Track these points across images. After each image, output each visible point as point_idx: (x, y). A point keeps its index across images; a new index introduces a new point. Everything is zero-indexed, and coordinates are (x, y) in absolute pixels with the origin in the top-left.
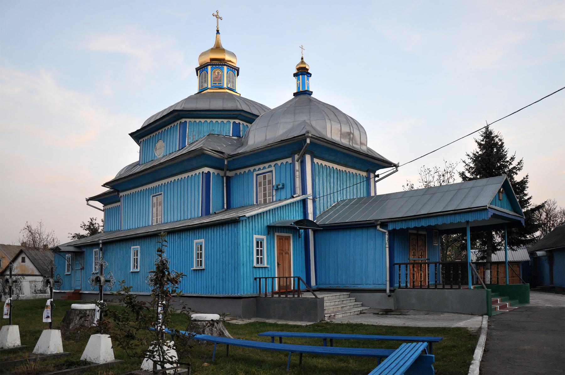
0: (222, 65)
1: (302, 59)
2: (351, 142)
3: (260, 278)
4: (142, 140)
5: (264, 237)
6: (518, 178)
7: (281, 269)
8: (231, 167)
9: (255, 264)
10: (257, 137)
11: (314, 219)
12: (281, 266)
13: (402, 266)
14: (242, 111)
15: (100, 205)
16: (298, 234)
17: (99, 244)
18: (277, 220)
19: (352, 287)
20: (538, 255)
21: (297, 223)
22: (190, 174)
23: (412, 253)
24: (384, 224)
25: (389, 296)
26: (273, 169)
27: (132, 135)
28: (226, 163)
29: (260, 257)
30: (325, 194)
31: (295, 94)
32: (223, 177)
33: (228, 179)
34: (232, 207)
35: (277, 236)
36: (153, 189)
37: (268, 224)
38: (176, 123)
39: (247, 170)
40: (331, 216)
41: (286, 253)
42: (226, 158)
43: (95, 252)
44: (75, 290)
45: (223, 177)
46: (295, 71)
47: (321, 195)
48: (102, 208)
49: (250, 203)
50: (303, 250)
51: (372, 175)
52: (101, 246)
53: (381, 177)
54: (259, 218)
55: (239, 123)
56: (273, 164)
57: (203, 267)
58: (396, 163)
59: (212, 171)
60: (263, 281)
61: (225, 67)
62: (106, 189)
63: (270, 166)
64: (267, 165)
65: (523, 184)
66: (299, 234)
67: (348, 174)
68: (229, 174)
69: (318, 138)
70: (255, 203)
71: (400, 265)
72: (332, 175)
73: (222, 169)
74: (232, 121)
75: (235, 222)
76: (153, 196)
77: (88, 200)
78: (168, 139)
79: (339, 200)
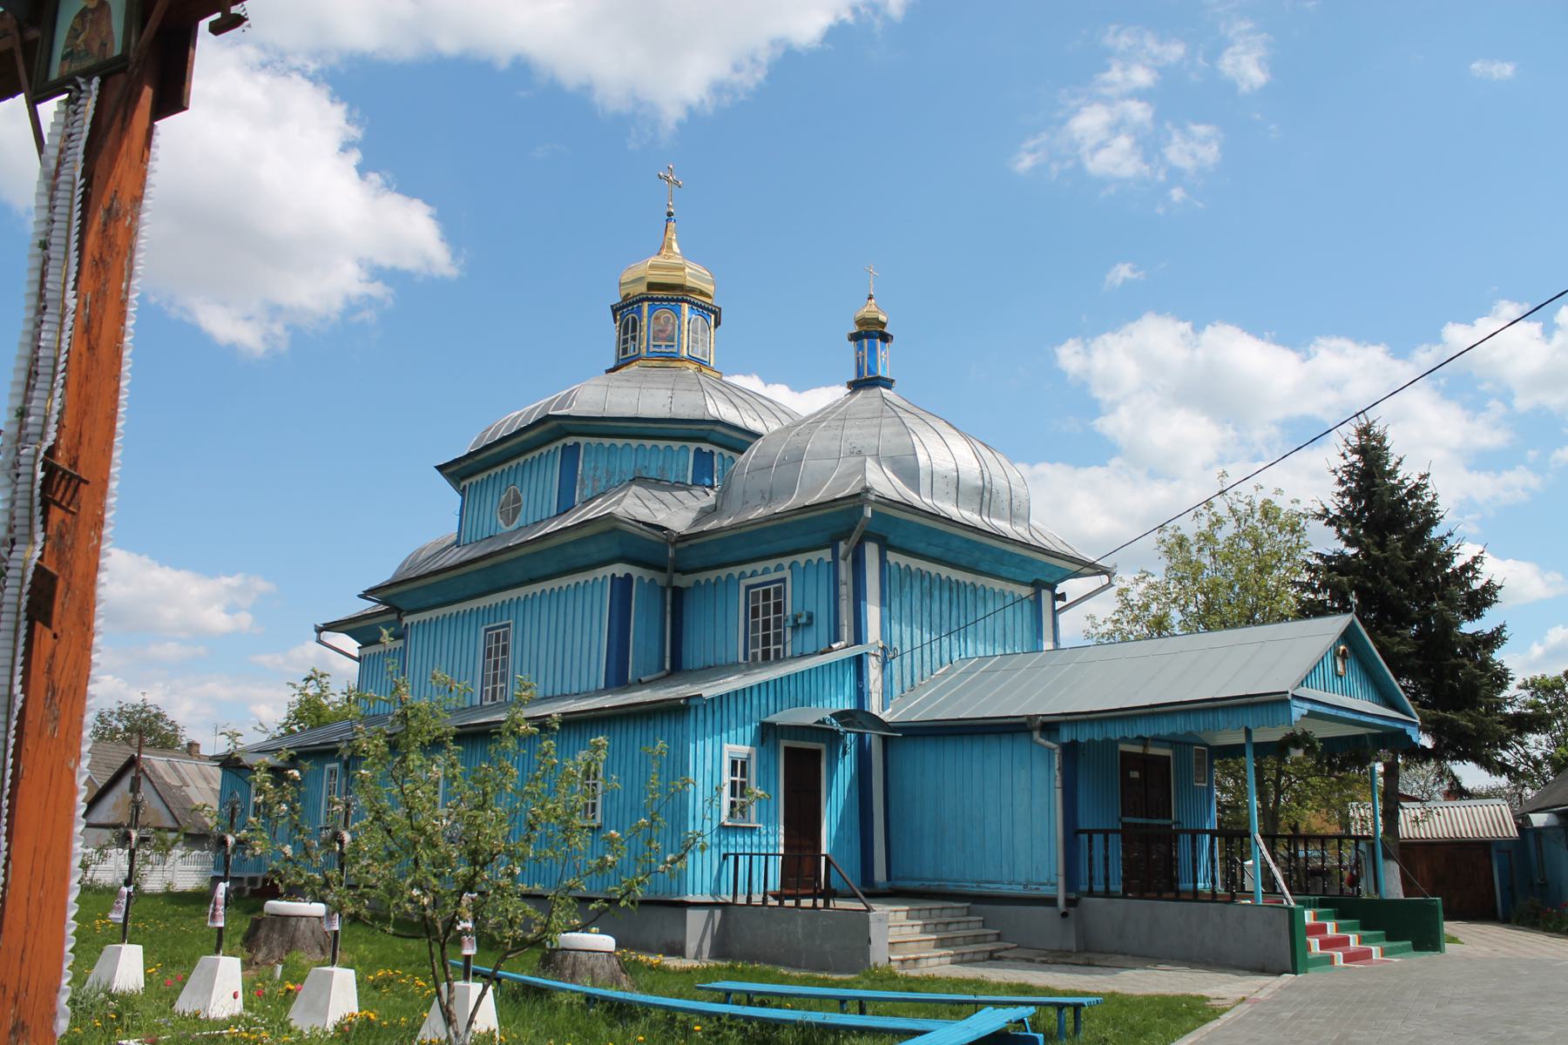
0: (678, 300)
4: (466, 483)
8: (671, 577)
14: (717, 422)
15: (351, 645)
19: (974, 889)
20: (1535, 824)
21: (841, 716)
24: (1050, 726)
25: (1064, 915)
26: (787, 573)
27: (440, 468)
28: (671, 553)
32: (663, 589)
33: (679, 594)
34: (684, 666)
35: (787, 749)
36: (489, 610)
38: (552, 447)
39: (723, 573)
40: (930, 699)
48: (356, 653)
49: (730, 660)
51: (1046, 595)
53: (1069, 600)
54: (709, 710)
56: (786, 561)
59: (635, 571)
61: (686, 306)
62: (367, 606)
63: (779, 568)
64: (772, 564)
67: (981, 592)
68: (682, 581)
70: (741, 659)
71: (1090, 833)
74: (693, 446)
75: (676, 711)
77: (319, 630)
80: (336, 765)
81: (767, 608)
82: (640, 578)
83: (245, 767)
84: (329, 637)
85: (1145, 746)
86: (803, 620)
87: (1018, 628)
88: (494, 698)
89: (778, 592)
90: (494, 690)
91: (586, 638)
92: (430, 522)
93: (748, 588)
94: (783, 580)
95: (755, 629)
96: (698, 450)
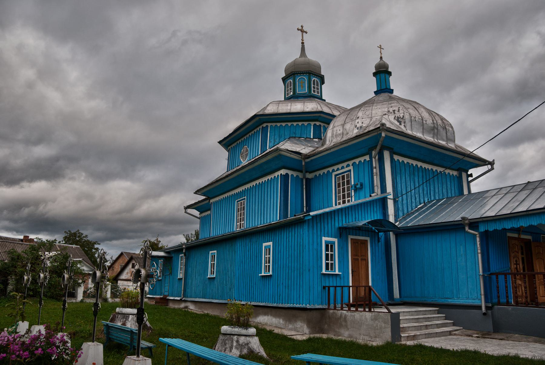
1: (381, 58)
3: (329, 287)
4: (230, 147)
5: (336, 240)
10: (334, 135)
11: (396, 221)
14: (322, 112)
15: (196, 213)
16: (376, 238)
17: (182, 249)
22: (269, 177)
25: (485, 314)
26: (351, 168)
27: (220, 142)
32: (302, 180)
33: (307, 180)
36: (237, 194)
37: (340, 225)
38: (258, 129)
39: (325, 171)
43: (181, 257)
44: (164, 295)
45: (302, 180)
47: (404, 192)
48: (198, 216)
50: (384, 256)
51: (464, 175)
52: (184, 251)
53: (474, 177)
55: (320, 125)
56: (351, 163)
57: (271, 273)
58: (491, 160)
59: (290, 173)
60: (332, 289)
63: (348, 166)
64: (345, 164)
66: (379, 238)
68: (309, 176)
71: (497, 275)
72: (416, 173)
76: (237, 202)
79: (426, 201)
80: (183, 255)
81: (343, 183)
82: (292, 175)
83: (360, 306)
84: (189, 211)
85: (519, 234)
86: (358, 186)
87: (453, 188)
88: (240, 228)
89: (348, 176)
90: (240, 224)
91: (272, 200)
92: (219, 166)
93: (336, 175)
94: (350, 171)
95: (339, 193)
96: (315, 125)
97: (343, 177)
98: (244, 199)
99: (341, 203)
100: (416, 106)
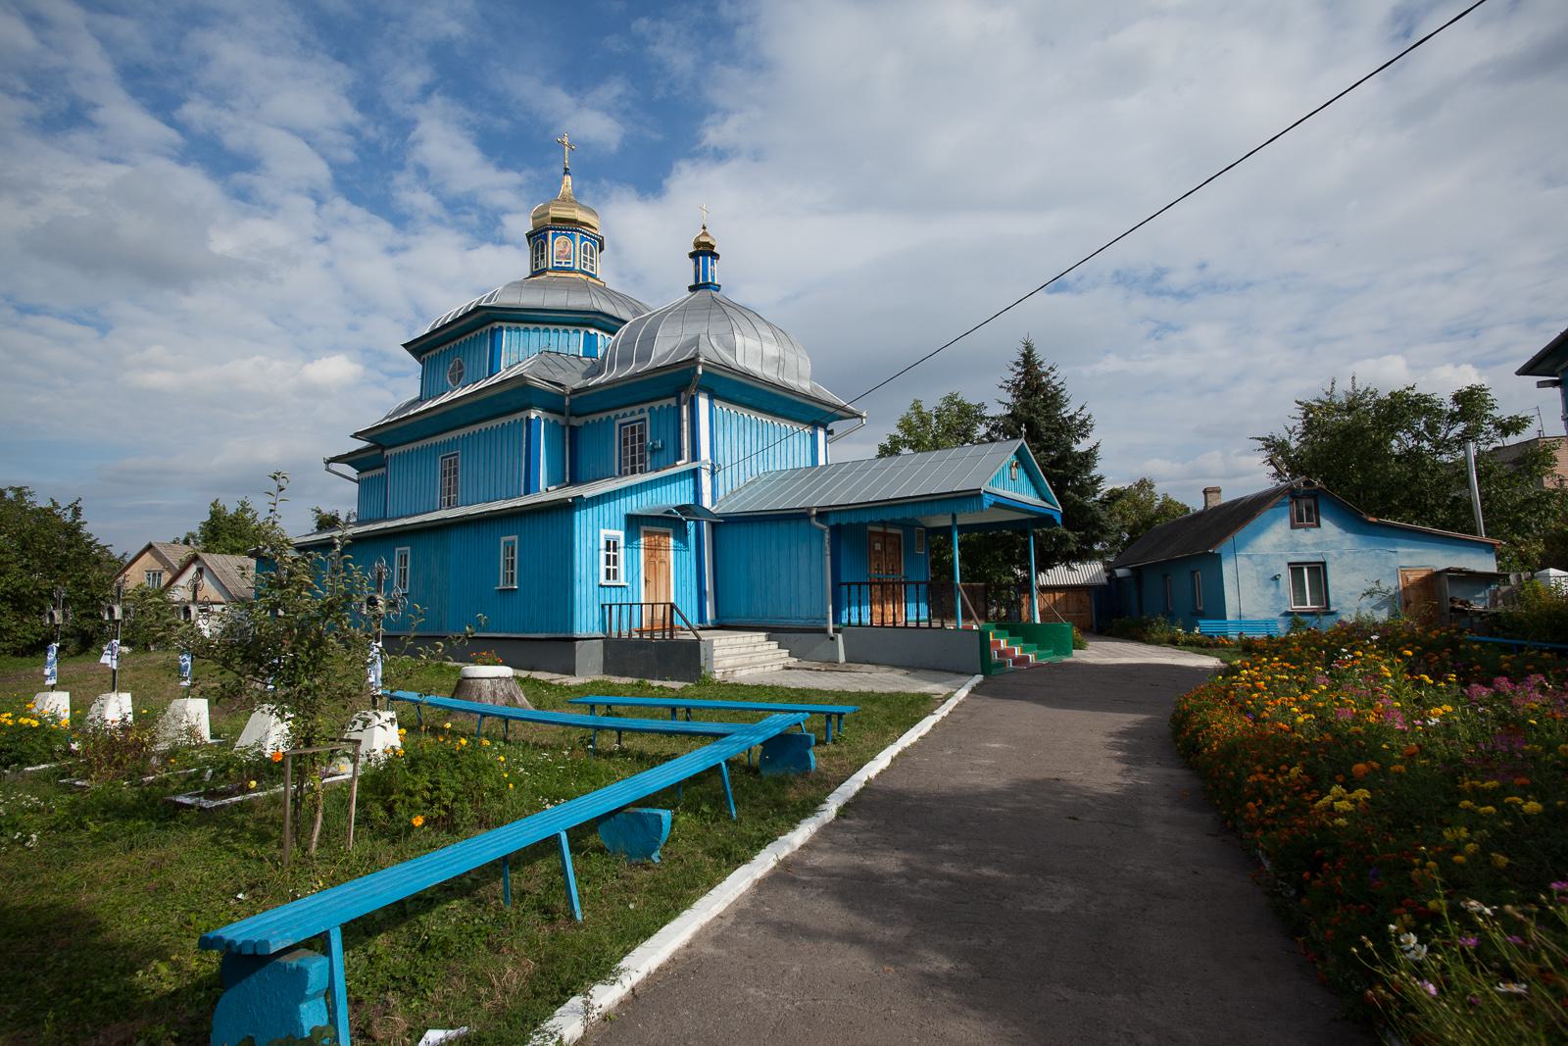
2: (780, 374)
6: (1081, 447)
7: (652, 589)
9: (603, 580)
12: (652, 585)
13: (852, 587)
14: (599, 313)
15: (352, 472)
18: (644, 503)
20: (1118, 576)
21: (681, 508)
22: (505, 420)
23: (874, 565)
26: (646, 415)
29: (611, 567)
30: (735, 460)
31: (692, 289)
32: (564, 427)
33: (572, 428)
37: (629, 512)
38: (484, 330)
39: (604, 416)
41: (661, 562)
42: (569, 395)
46: (692, 250)
47: (728, 463)
56: (646, 407)
62: (363, 444)
63: (641, 411)
64: (636, 409)
65: (1088, 459)
68: (575, 422)
69: (717, 366)
70: (617, 474)
71: (849, 585)
72: (748, 429)
73: (562, 414)
78: (471, 358)
79: (761, 471)
81: (633, 439)
84: (334, 466)
90: (449, 499)
92: (400, 389)
93: (621, 425)
94: (644, 420)
97: (633, 429)
98: (457, 454)
99: (629, 471)
100: (749, 315)
